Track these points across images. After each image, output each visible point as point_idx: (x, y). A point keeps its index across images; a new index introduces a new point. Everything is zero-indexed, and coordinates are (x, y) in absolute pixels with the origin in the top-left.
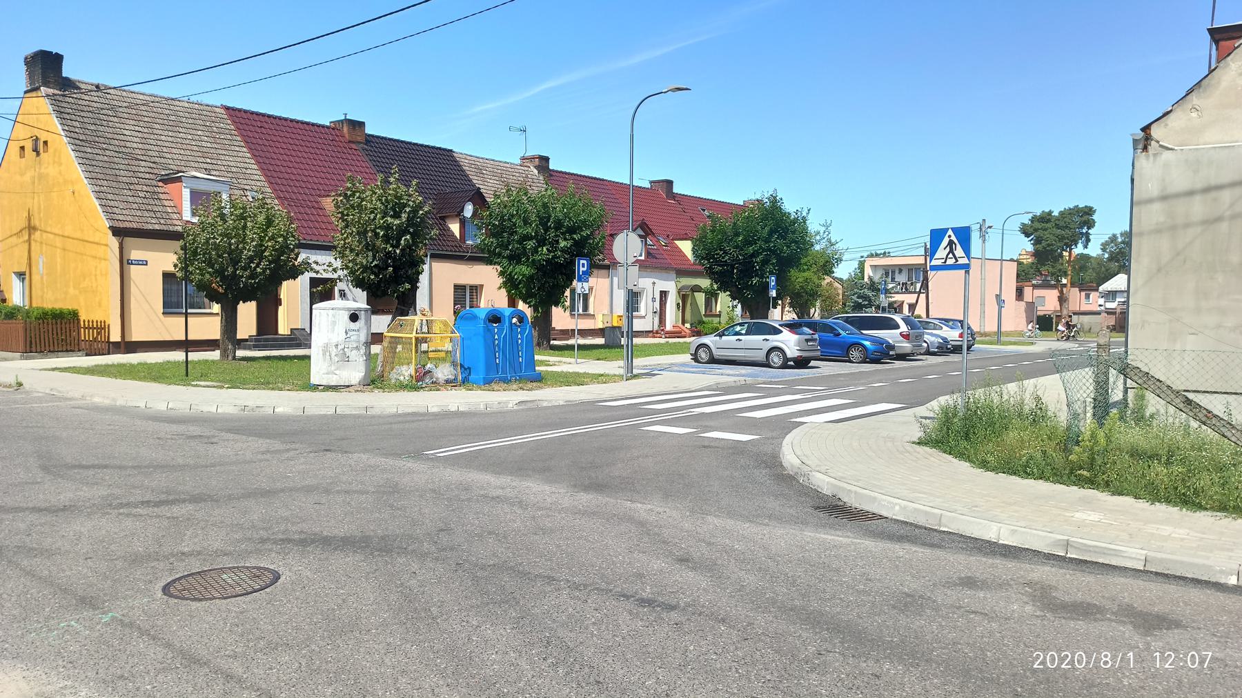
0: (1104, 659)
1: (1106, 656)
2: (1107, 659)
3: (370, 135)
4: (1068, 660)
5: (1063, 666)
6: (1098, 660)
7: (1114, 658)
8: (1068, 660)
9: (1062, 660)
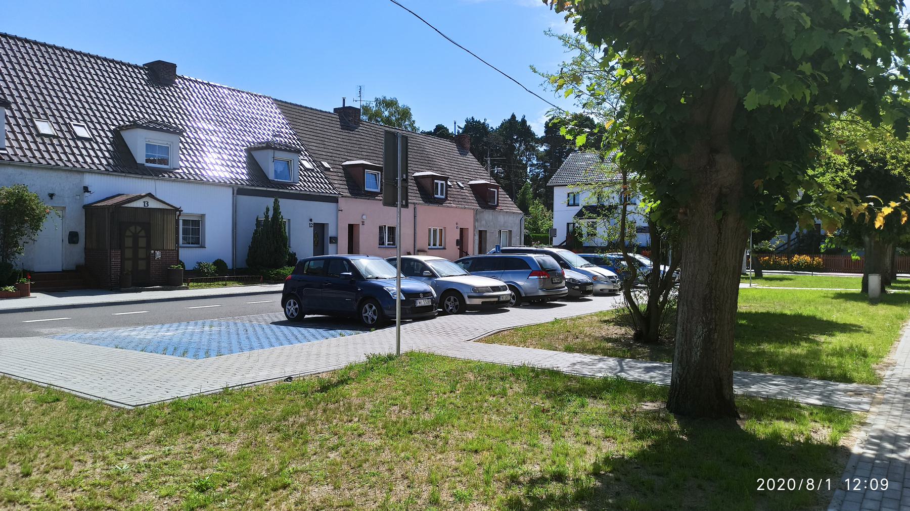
0: (809, 484)
2: (811, 484)
5: (779, 489)
7: (816, 484)
9: (778, 485)
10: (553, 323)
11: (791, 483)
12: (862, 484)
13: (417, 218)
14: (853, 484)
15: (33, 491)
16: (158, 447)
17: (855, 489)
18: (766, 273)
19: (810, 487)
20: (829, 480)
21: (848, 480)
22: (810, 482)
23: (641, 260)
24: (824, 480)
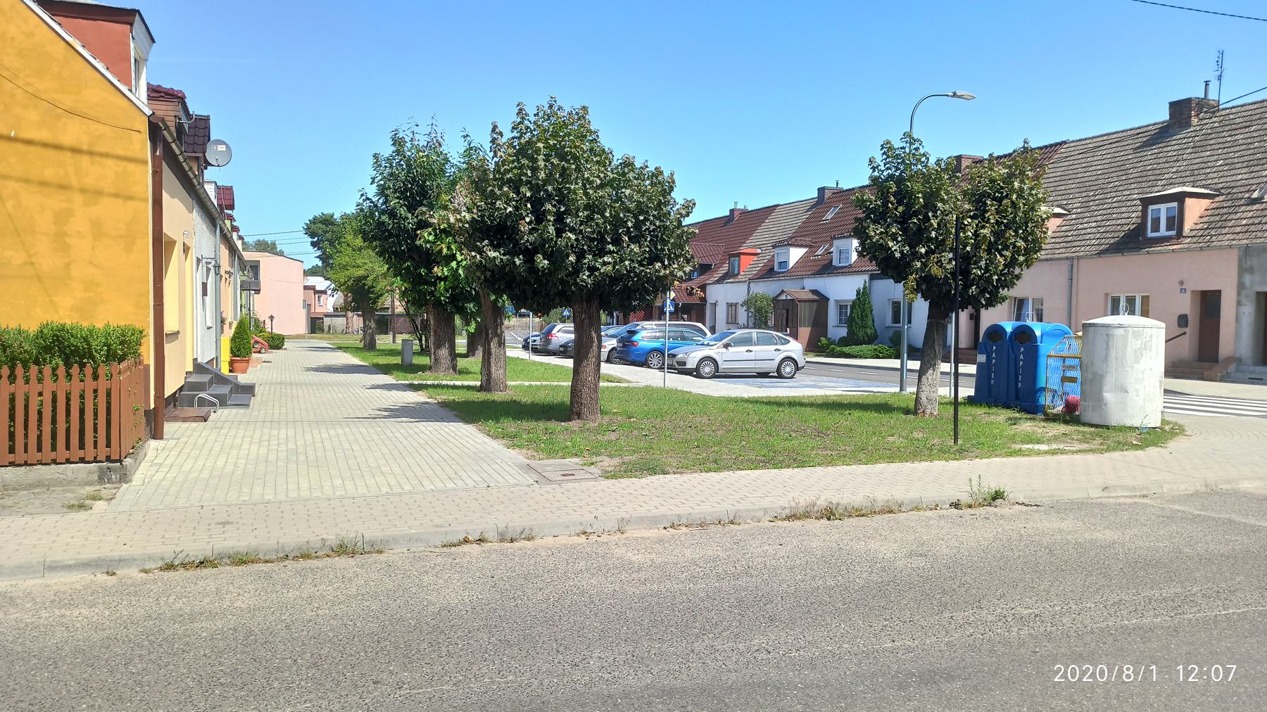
0: (1127, 672)
1: (1128, 669)
2: (1130, 672)
3: (899, 358)
4: (1061, 673)
6: (1121, 671)
7: (1136, 673)
8: (1061, 673)
9: (1083, 673)
10: (516, 358)
11: (1217, 670)
12: (1201, 673)
13: (46, 27)
14: (1187, 674)
15: (604, 150)
16: (442, 361)
17: (1190, 680)
18: (736, 272)
19: (1128, 676)
20: (1154, 667)
21: (1181, 667)
22: (1128, 670)
23: (392, 358)
24: (1147, 667)
